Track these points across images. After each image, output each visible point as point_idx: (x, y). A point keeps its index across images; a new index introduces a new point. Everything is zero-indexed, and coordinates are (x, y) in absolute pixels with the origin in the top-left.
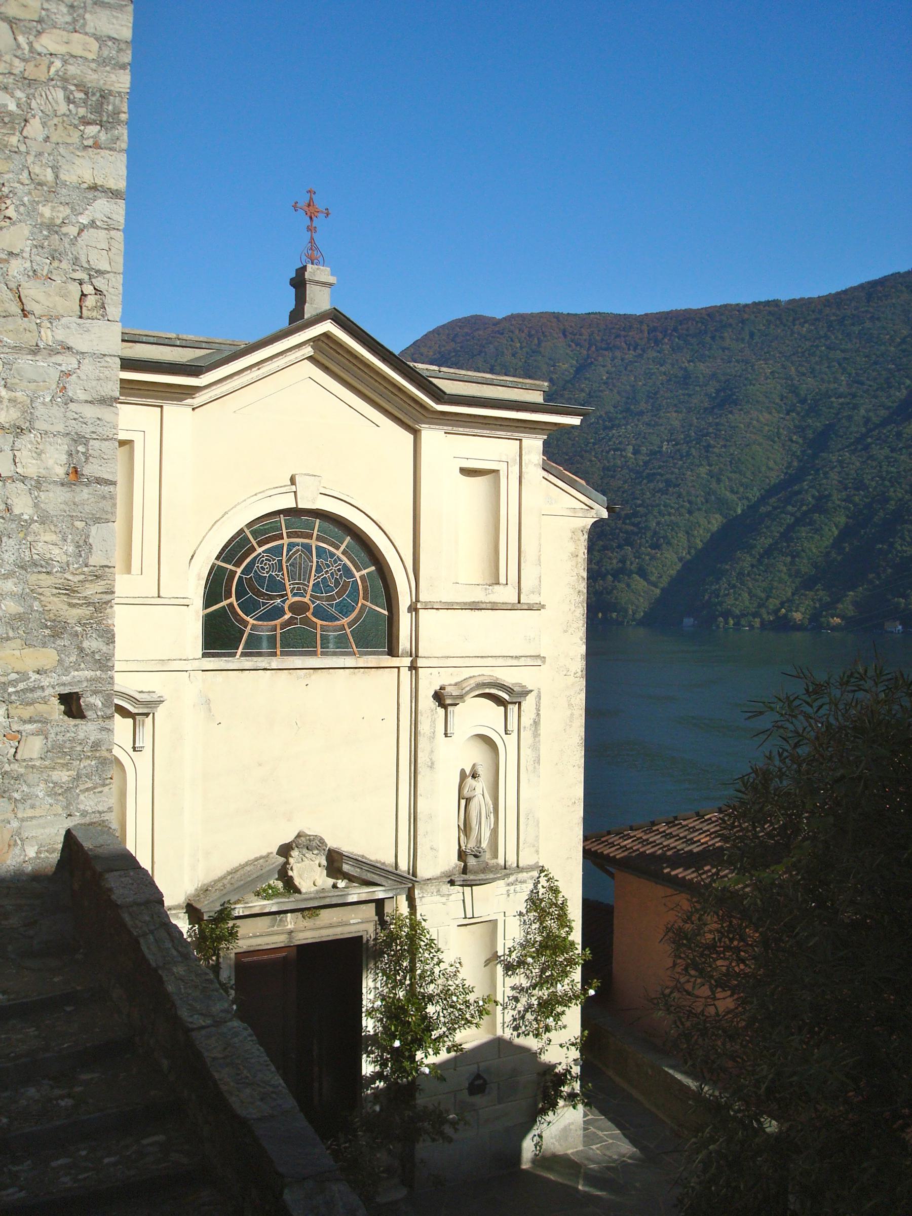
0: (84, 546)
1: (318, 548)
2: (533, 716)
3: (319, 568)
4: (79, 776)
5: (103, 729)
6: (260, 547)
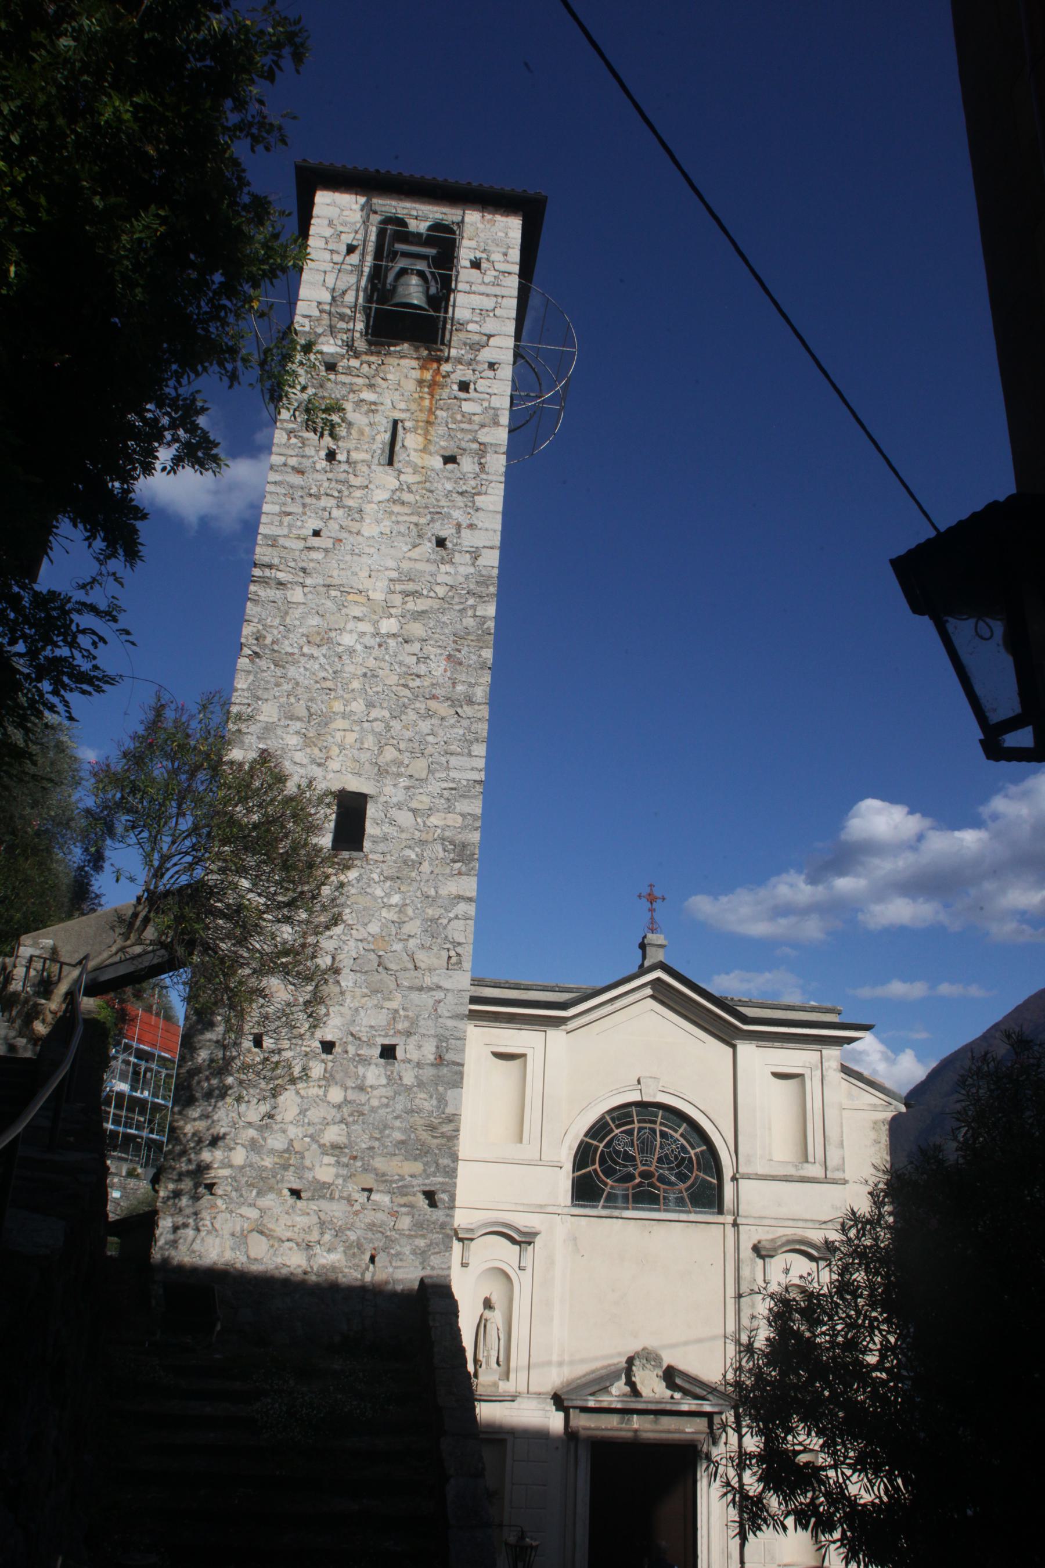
0: (442, 1100)
1: (661, 1131)
3: (661, 1148)
4: (431, 1244)
5: (447, 1215)
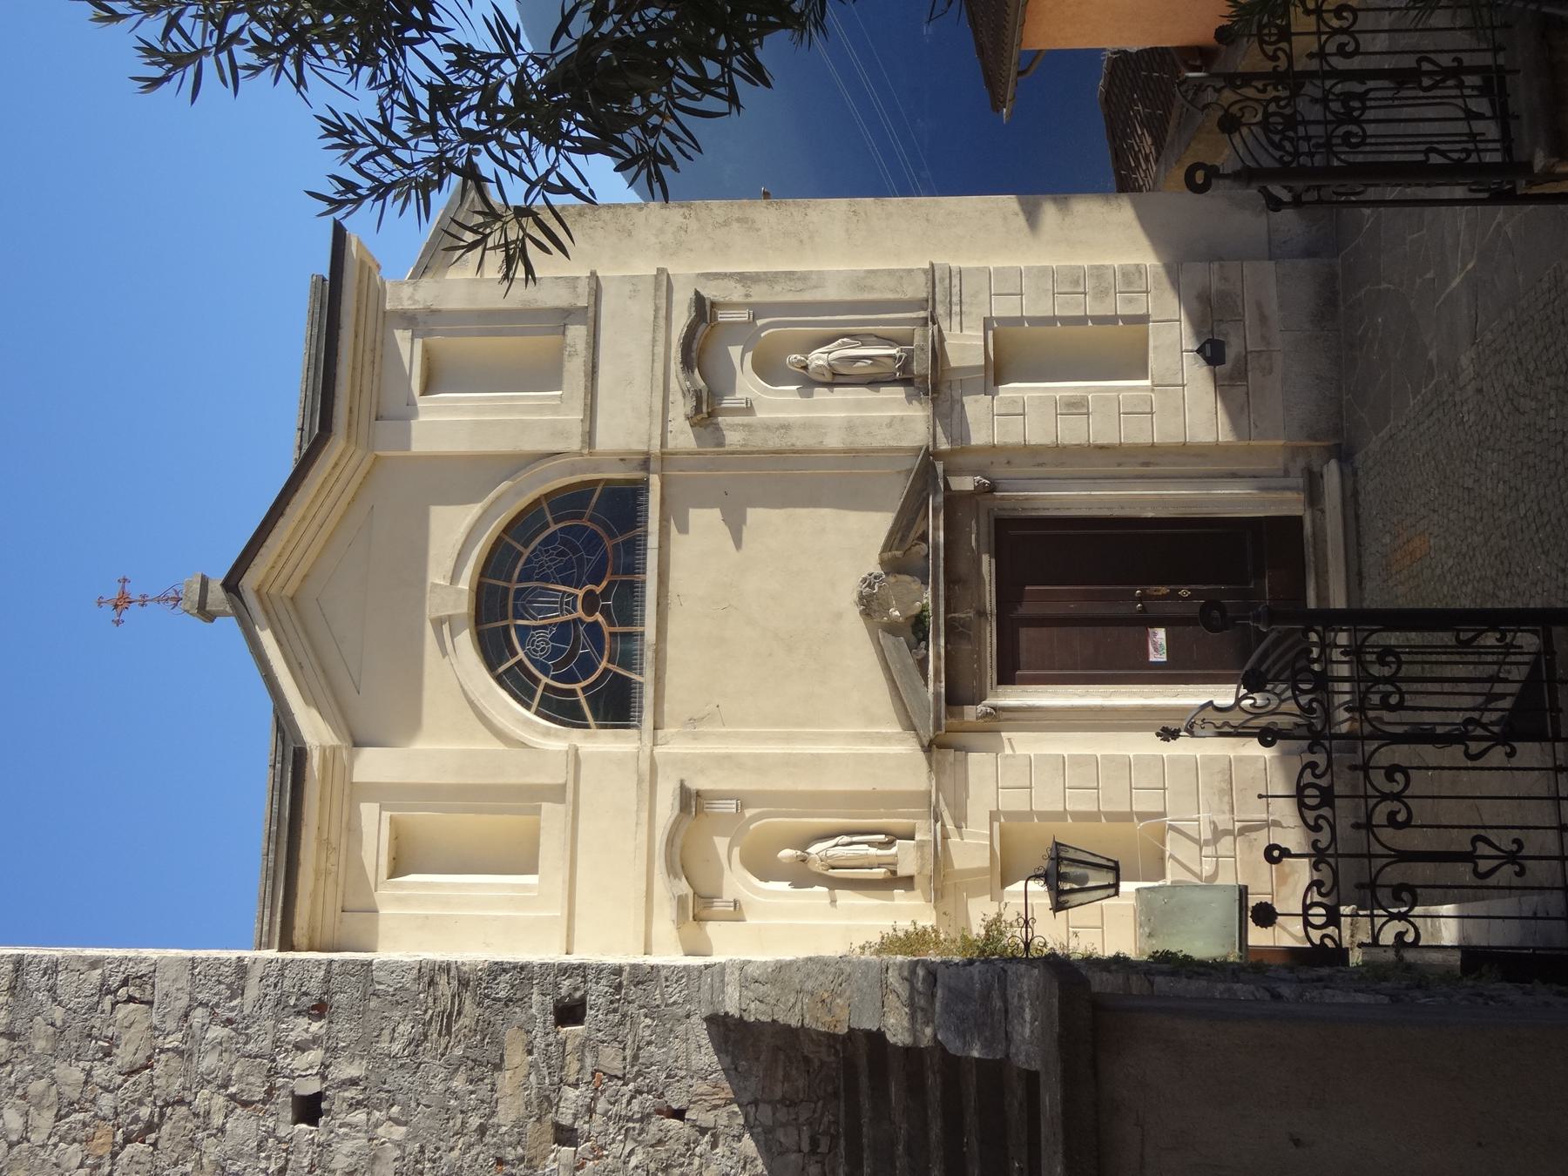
0: (398, 999)
1: (520, 580)
2: (732, 284)
6: (517, 654)
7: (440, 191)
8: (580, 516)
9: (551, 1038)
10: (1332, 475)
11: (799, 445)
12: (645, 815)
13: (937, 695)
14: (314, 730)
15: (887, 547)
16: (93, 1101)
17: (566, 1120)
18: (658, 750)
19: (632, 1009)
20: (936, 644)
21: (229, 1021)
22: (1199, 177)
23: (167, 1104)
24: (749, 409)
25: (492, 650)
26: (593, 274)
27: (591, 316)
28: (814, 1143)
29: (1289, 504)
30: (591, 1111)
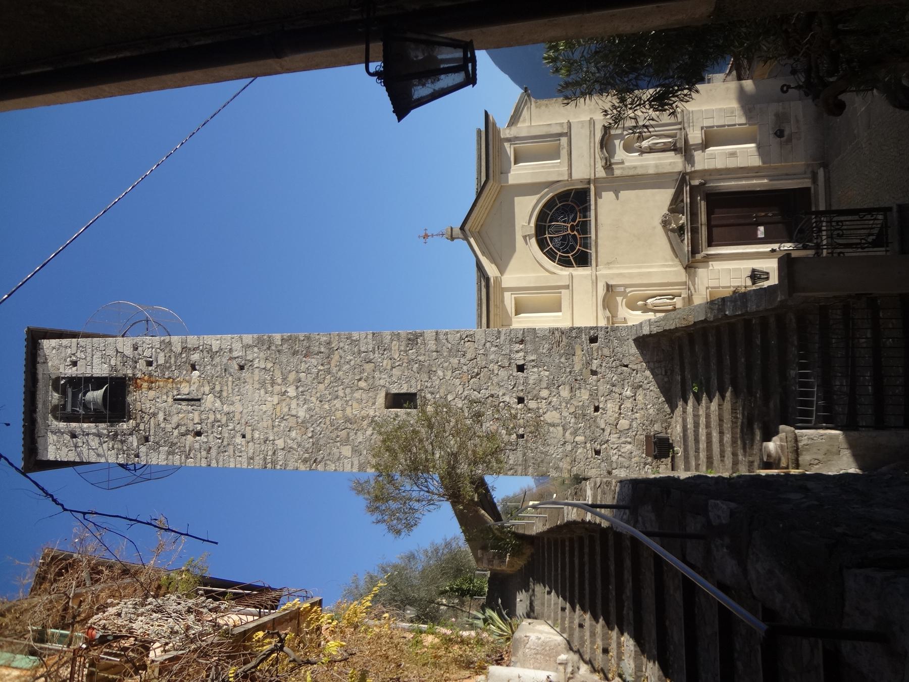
0: (544, 338)
1: (549, 223)
7: (473, 86)
8: (568, 201)
9: (589, 347)
10: (821, 173)
11: (640, 173)
12: (595, 293)
13: (688, 251)
14: (491, 270)
15: (671, 204)
16: (461, 368)
17: (594, 369)
18: (597, 273)
19: (611, 338)
20: (688, 235)
21: (497, 346)
22: (785, 88)
23: (482, 368)
24: (622, 163)
25: (542, 244)
26: (569, 121)
27: (568, 135)
28: (666, 372)
29: (806, 183)
30: (601, 366)
